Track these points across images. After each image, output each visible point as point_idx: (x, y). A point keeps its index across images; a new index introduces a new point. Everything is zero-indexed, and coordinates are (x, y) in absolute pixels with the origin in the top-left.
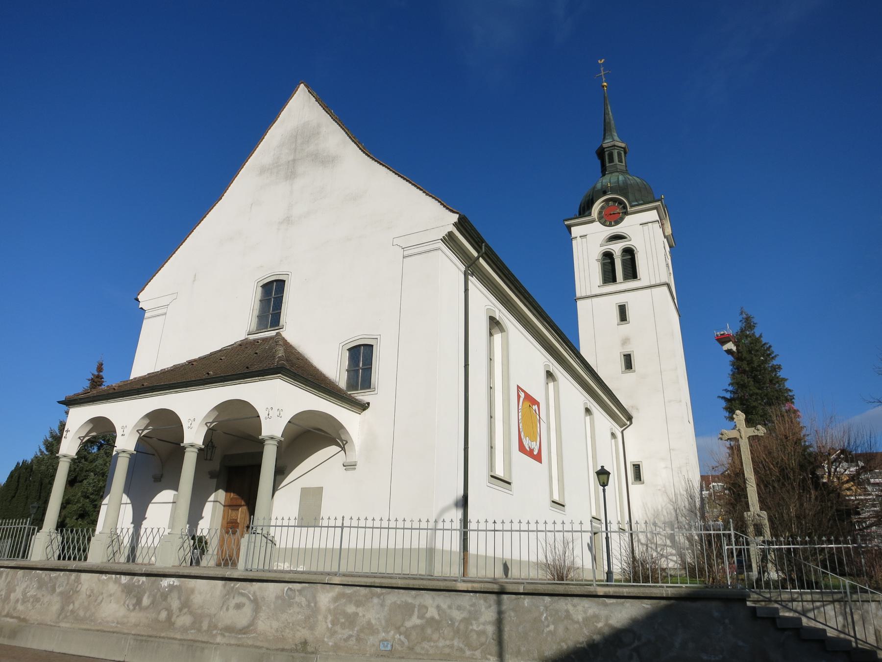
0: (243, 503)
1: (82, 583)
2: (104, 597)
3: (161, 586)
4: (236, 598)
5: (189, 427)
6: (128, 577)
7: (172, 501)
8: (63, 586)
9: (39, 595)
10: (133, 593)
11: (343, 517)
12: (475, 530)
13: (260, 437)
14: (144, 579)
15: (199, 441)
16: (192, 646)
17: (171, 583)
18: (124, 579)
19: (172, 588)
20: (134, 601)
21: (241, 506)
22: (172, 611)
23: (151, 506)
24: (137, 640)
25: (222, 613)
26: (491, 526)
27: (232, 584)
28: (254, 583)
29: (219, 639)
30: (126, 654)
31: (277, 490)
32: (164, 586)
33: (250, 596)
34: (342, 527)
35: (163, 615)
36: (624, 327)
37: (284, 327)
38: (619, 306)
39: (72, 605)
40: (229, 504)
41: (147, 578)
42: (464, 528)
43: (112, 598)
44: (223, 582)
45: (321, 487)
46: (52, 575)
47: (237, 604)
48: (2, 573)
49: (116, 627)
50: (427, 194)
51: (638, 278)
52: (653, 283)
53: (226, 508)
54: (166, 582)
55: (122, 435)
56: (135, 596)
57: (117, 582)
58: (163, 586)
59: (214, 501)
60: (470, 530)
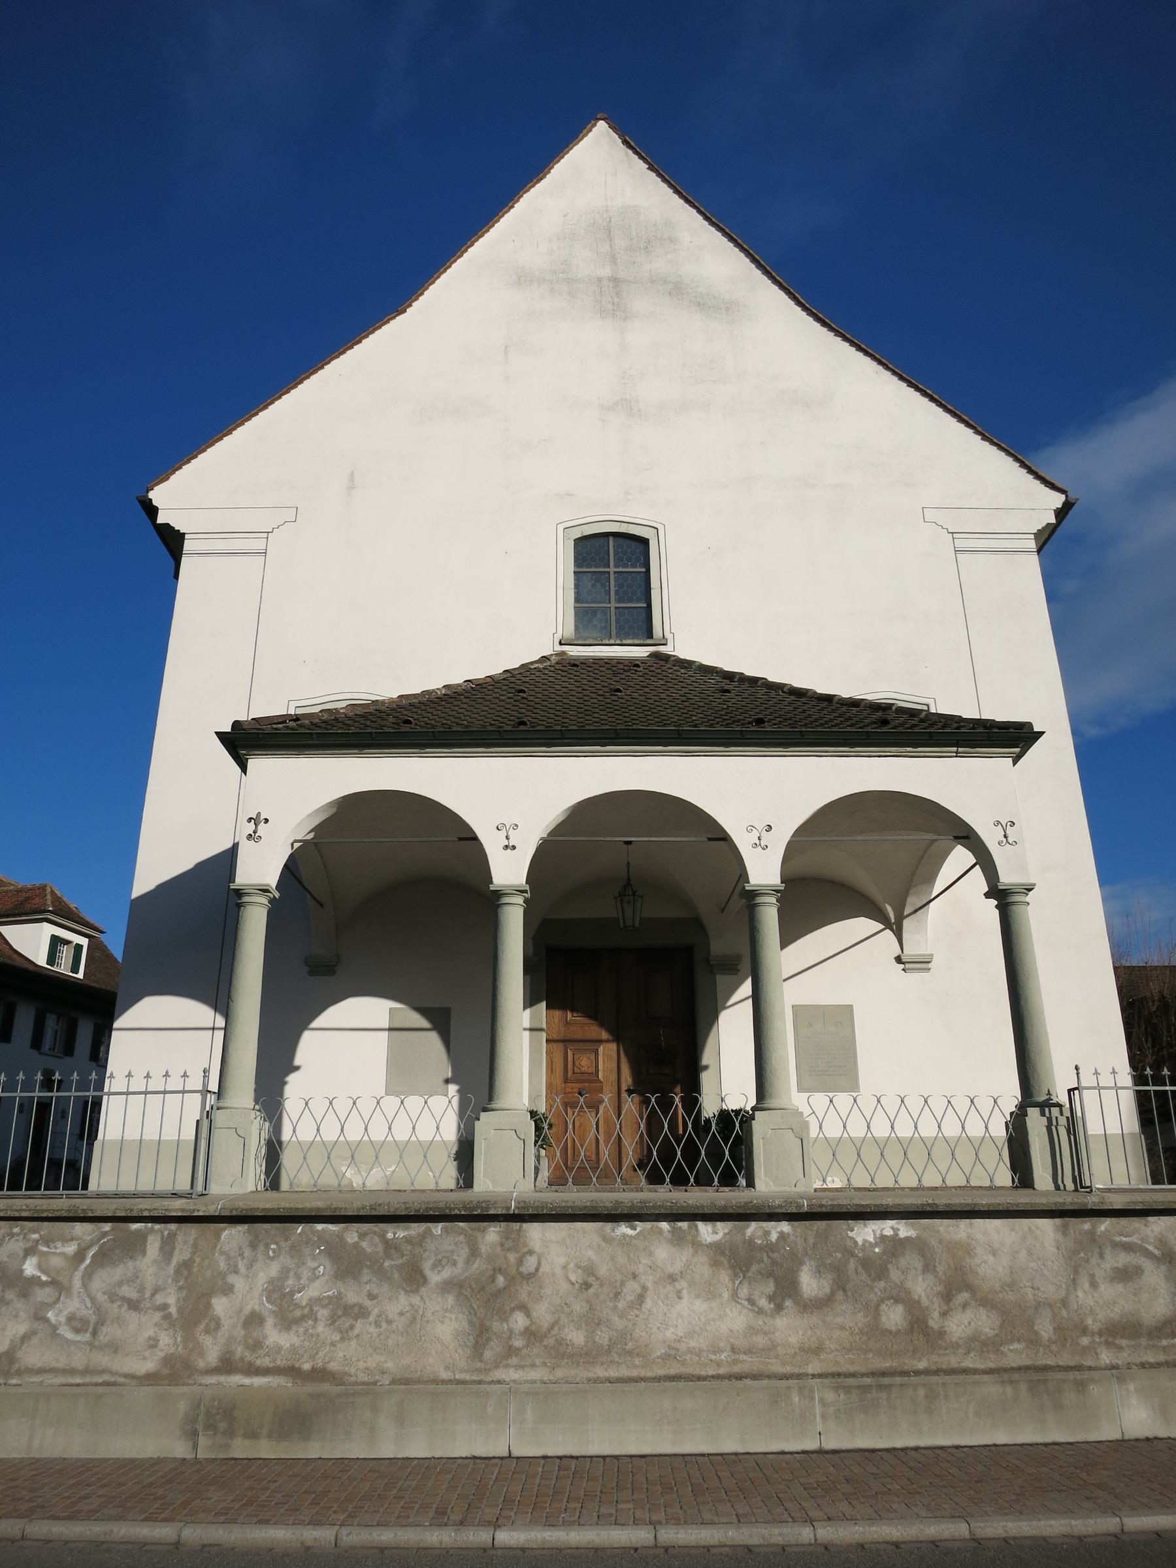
0: (604, 1035)
1: (537, 1248)
2: (649, 1284)
3: (856, 1243)
4: (1108, 1257)
6: (723, 1228)
7: (387, 1027)
8: (455, 1264)
9: (353, 1296)
10: (755, 1268)
13: (492, 888)
14: (785, 1227)
15: (271, 878)
16: (1045, 1382)
17: (888, 1232)
18: (707, 1232)
19: (895, 1246)
20: (770, 1287)
21: (601, 1041)
22: (919, 1302)
23: (307, 1038)
24: (848, 1389)
25: (1080, 1294)
27: (1086, 1225)
28: (1151, 1219)
29: (1106, 1357)
30: (819, 1429)
31: (725, 1008)
32: (865, 1241)
33: (1151, 1248)
35: (894, 1317)
40: (561, 1037)
41: (795, 1223)
43: (682, 1284)
44: (1058, 1221)
45: (447, 1008)
46: (390, 1235)
47: (1116, 1270)
48: (142, 1237)
49: (735, 1362)
50: (984, 438)
53: (555, 1045)
54: (866, 1233)
55: (506, 847)
56: (770, 1275)
57: (678, 1239)
58: (860, 1243)
59: (390, 1029)
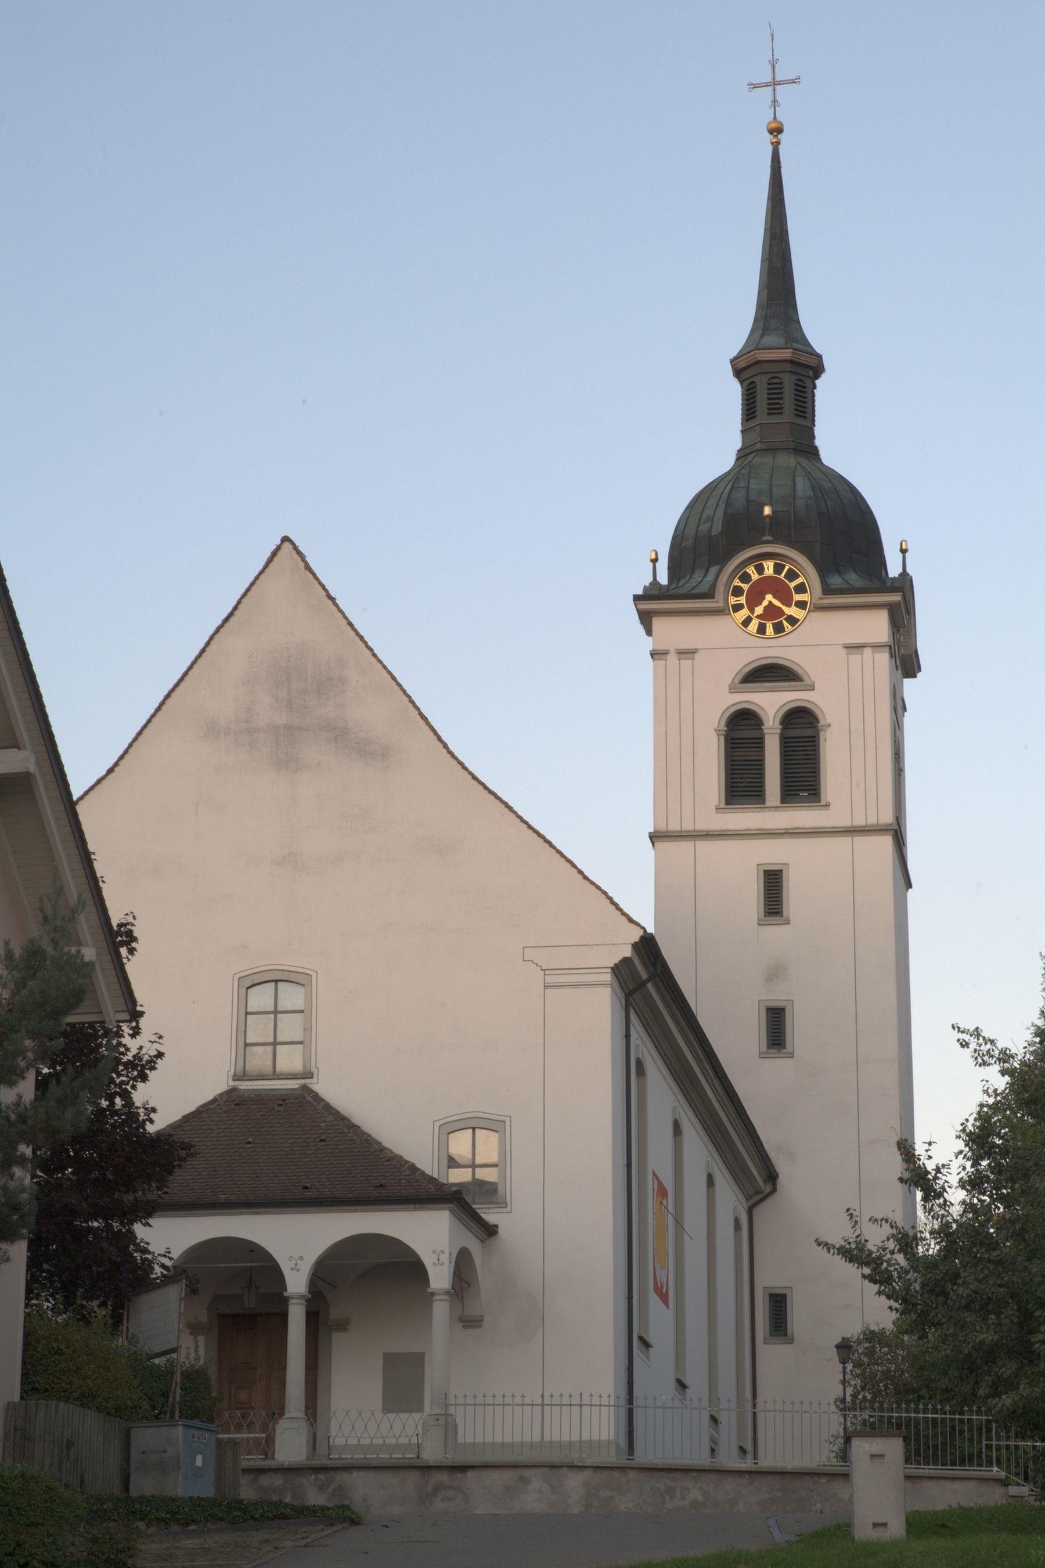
5: (292, 1269)
11: (581, 1394)
12: (549, 1405)
26: (518, 1400)
34: (543, 1405)
36: (774, 932)
37: (315, 1076)
38: (765, 871)
39: (997, 1399)
42: (629, 1404)
51: (823, 803)
52: (860, 821)
60: (637, 1407)
